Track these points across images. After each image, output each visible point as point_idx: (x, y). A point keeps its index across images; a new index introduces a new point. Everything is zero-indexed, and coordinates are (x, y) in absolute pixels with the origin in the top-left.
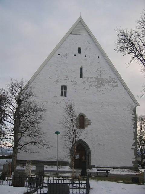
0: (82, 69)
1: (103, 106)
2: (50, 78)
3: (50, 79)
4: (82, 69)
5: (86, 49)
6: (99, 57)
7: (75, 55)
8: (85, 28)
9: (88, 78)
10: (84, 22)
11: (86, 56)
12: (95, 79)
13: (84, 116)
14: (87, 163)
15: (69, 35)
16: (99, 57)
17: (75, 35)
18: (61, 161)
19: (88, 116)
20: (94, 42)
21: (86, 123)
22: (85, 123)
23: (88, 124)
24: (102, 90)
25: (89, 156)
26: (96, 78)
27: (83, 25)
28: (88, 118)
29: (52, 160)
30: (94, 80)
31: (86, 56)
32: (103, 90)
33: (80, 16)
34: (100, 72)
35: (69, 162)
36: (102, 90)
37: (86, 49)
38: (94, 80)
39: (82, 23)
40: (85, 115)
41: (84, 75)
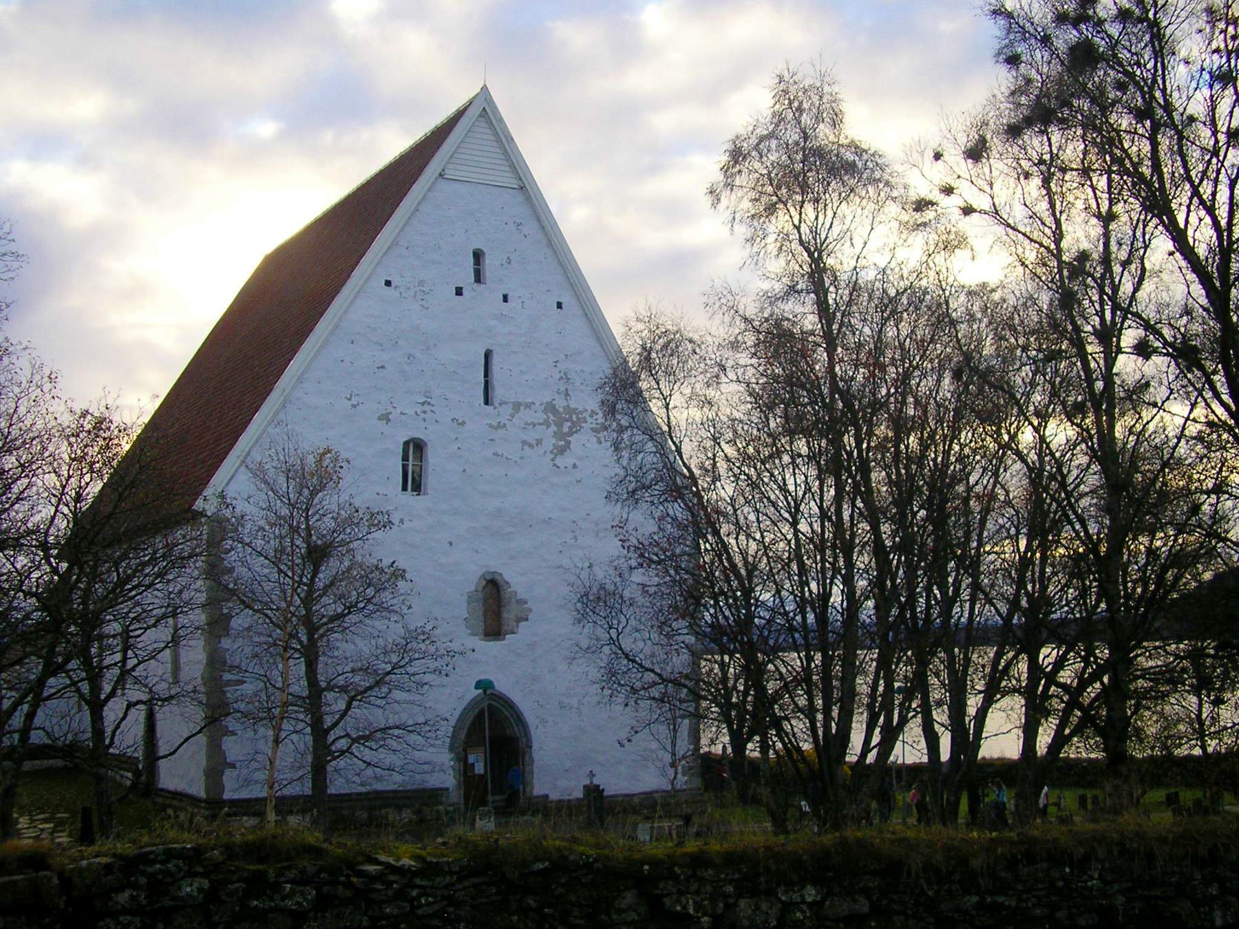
0: (488, 355)
1: (576, 538)
2: (354, 401)
3: (354, 406)
4: (488, 355)
5: (509, 261)
6: (559, 305)
7: (459, 292)
8: (506, 150)
9: (517, 406)
10: (501, 120)
11: (505, 298)
12: (545, 411)
13: (501, 582)
14: (649, 840)
15: (433, 183)
16: (559, 305)
17: (457, 186)
18: (414, 787)
19: (516, 580)
20: (539, 220)
21: (508, 615)
22: (505, 615)
23: (520, 620)
24: (575, 466)
25: (527, 758)
26: (550, 408)
27: (322, 347)
28: (519, 591)
29: (379, 786)
30: (541, 417)
31: (505, 298)
32: (578, 463)
33: (485, 89)
34: (566, 378)
35: (447, 789)
36: (575, 466)
37: (509, 261)
38: (541, 417)
39: (398, 235)
40: (506, 577)
41: (498, 393)
